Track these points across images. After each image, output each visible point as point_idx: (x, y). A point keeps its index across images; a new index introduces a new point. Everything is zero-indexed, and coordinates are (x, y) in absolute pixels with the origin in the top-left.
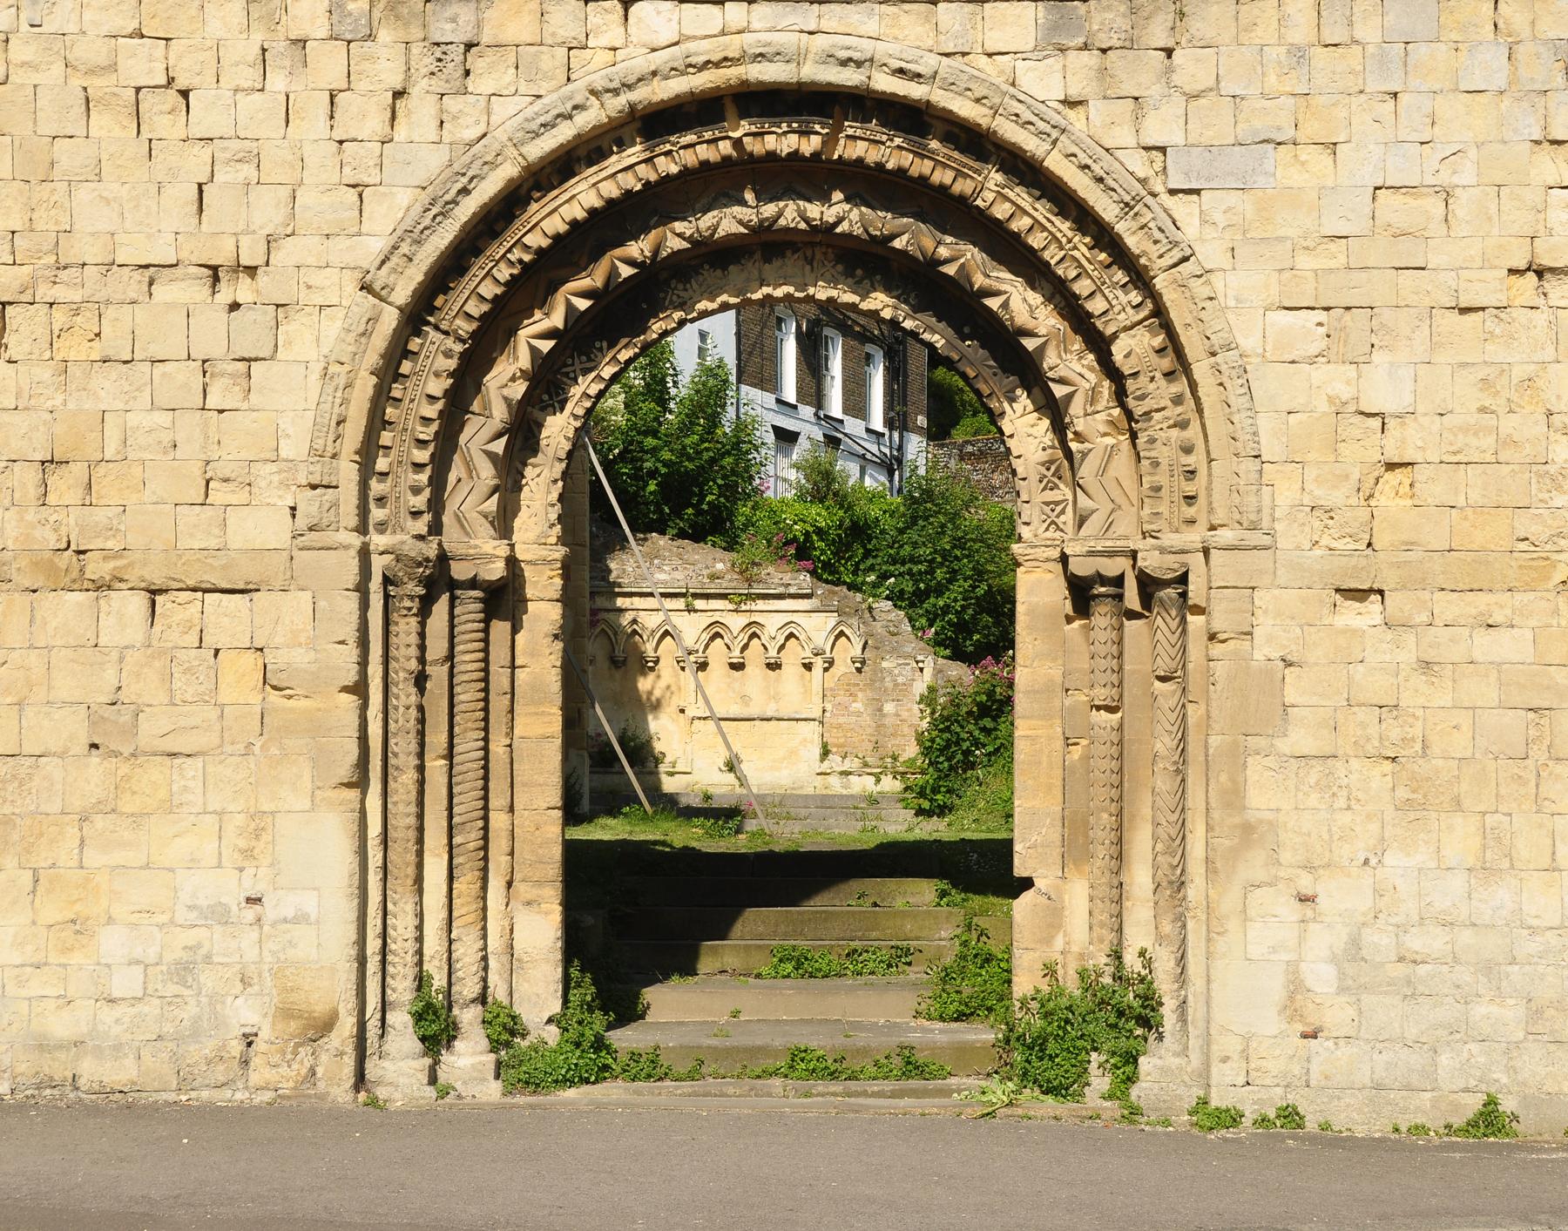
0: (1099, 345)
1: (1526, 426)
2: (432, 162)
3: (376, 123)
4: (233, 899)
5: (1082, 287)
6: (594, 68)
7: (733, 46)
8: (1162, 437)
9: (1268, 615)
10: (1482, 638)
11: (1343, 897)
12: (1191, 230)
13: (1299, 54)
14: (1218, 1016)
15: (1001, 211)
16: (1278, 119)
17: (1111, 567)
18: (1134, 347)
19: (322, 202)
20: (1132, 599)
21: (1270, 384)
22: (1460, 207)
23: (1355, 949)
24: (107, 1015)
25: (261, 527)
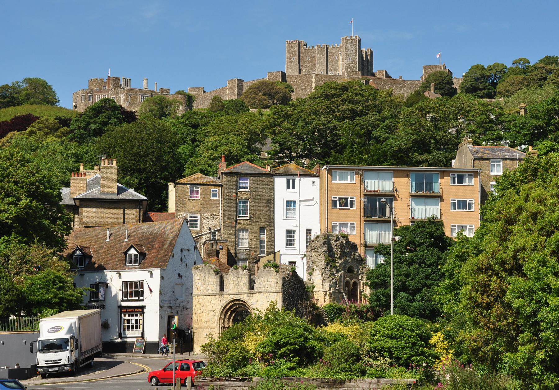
19: (218, 307)
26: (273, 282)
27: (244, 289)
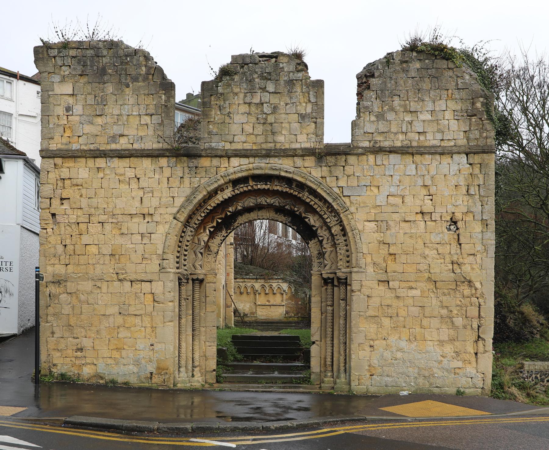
0: (329, 229)
5: (325, 216)
6: (222, 171)
7: (251, 166)
8: (342, 250)
9: (366, 287)
12: (348, 203)
15: (308, 200)
18: (336, 230)
22: (408, 199)
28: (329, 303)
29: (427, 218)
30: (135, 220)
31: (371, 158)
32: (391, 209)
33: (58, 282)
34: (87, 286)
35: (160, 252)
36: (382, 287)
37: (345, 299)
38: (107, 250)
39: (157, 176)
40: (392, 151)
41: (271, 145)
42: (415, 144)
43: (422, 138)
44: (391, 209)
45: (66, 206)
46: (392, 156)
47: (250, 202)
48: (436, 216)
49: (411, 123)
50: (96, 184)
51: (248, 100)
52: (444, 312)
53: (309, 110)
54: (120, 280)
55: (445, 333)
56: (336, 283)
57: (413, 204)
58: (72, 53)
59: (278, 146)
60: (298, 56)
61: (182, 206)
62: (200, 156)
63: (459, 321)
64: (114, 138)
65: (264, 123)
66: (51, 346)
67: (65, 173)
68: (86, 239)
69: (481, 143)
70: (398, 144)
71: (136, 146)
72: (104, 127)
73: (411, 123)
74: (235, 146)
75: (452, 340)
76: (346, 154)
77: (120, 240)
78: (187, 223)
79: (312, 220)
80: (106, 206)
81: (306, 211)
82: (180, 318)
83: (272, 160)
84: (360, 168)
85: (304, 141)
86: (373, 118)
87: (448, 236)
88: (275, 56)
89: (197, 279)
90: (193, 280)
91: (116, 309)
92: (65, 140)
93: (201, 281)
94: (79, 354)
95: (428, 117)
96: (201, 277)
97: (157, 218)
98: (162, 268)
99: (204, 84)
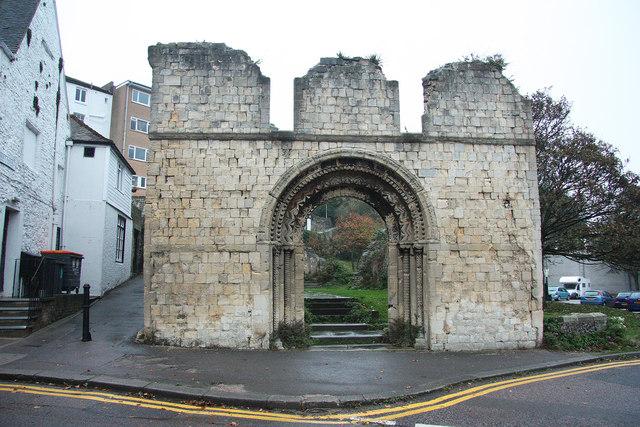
0: (406, 205)
1: (483, 220)
2: (283, 171)
3: (272, 164)
4: (246, 312)
5: (403, 195)
6: (313, 153)
7: (339, 150)
8: (418, 224)
9: (441, 258)
10: (477, 260)
11: (453, 307)
12: (423, 184)
13: (441, 154)
14: (432, 330)
15: (388, 180)
16: (438, 165)
17: (408, 247)
18: (412, 206)
19: (263, 179)
20: (412, 253)
21: (439, 213)
22: (470, 182)
23: (456, 317)
24: (223, 334)
25: (251, 240)
26: (499, 114)
27: (382, 127)
28: (406, 270)
29: (487, 197)
30: (233, 196)
31: (440, 145)
32: (459, 189)
33: (160, 253)
34: (188, 256)
35: (257, 225)
36: (455, 256)
37: (421, 267)
38: (207, 223)
39: (254, 157)
40: (457, 140)
41: (357, 133)
42: (474, 136)
43: (479, 131)
44: (459, 189)
45: (170, 182)
46: (457, 144)
47: (336, 181)
48: (494, 196)
49: (469, 119)
50: (199, 163)
51: (335, 93)
52: (505, 277)
53: (387, 105)
54: (220, 251)
55: (507, 294)
56: (412, 253)
57: (474, 186)
58: (181, 52)
59: (363, 133)
60: (374, 61)
61: (278, 184)
62: (295, 140)
63: (516, 284)
64: (216, 124)
65: (349, 114)
66: (155, 312)
67: (170, 154)
68: (188, 214)
69: (525, 137)
70: (461, 135)
71: (236, 131)
72: (207, 113)
73: (469, 119)
74: (324, 132)
75: (511, 301)
76: (419, 142)
77: (221, 215)
78: (280, 199)
79: (390, 197)
80: (207, 183)
81: (385, 190)
82: (274, 286)
83: (357, 145)
84: (431, 152)
85: (384, 130)
86: (440, 114)
87: (505, 212)
88: (358, 60)
89: (289, 250)
90: (285, 251)
91: (216, 278)
92: (172, 125)
93: (292, 252)
94: (181, 320)
95: (482, 114)
96: (292, 248)
97: (253, 194)
98: (259, 241)
99: (296, 80)
